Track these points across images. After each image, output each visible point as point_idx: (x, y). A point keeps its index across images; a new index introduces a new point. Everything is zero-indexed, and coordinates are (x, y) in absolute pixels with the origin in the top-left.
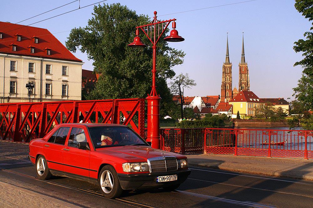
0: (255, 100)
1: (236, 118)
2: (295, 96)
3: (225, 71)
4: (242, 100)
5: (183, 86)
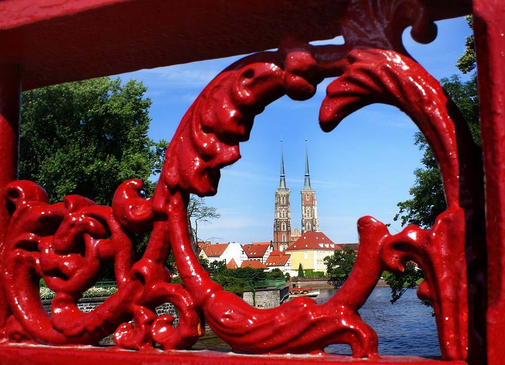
0: (327, 246)
1: (286, 95)
2: (400, 221)
3: (280, 201)
4: (306, 246)
5: (196, 218)
